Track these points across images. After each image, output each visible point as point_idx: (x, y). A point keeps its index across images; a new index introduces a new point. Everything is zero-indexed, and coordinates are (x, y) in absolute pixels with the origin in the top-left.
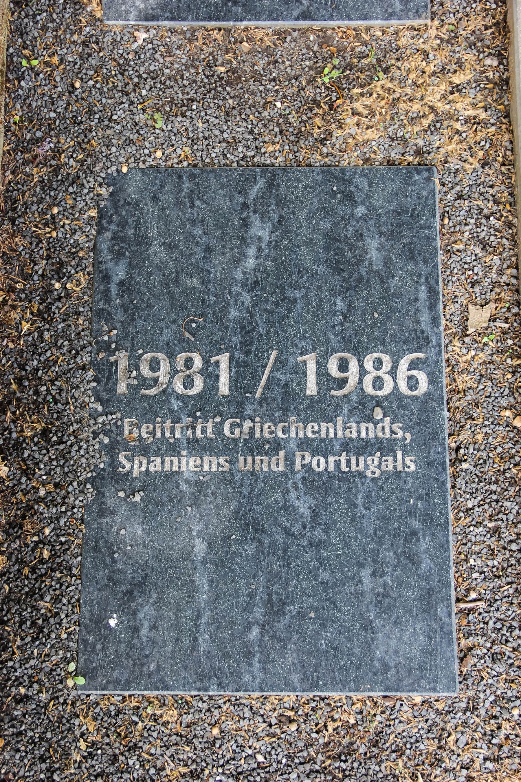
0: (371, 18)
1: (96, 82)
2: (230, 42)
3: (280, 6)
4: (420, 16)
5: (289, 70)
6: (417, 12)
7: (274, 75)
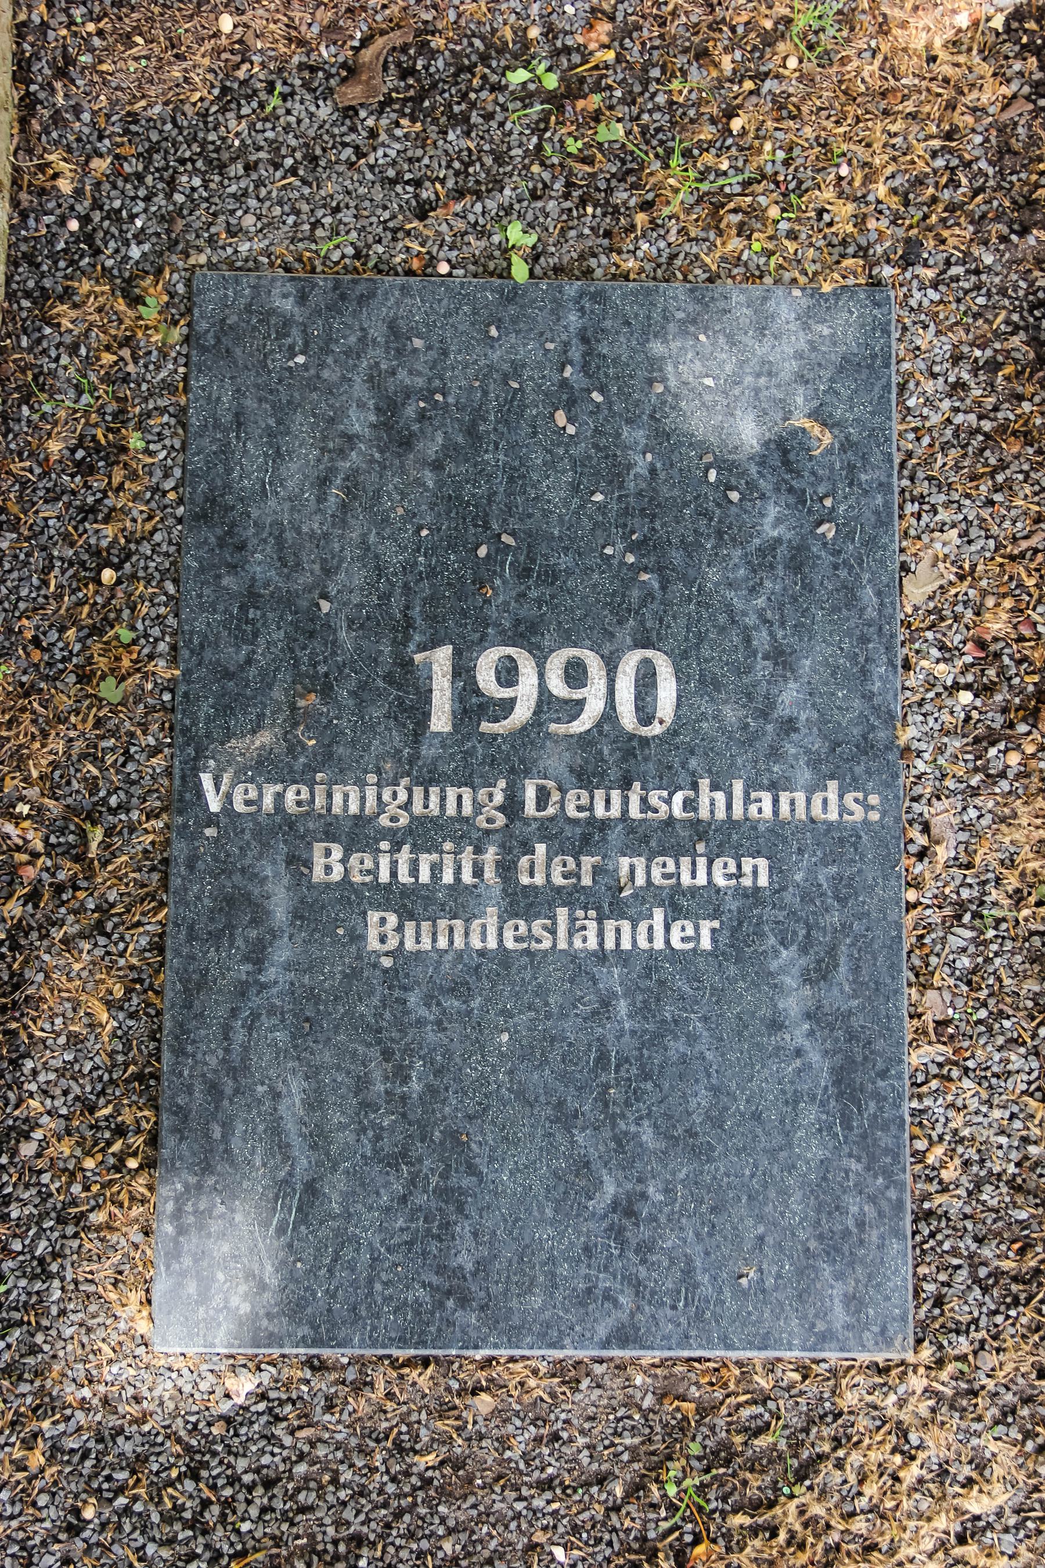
0: (778, 1345)
1: (135, 1499)
2: (448, 1389)
3: (567, 1311)
4: (889, 1343)
5: (584, 1457)
6: (883, 1331)
7: (550, 1470)
